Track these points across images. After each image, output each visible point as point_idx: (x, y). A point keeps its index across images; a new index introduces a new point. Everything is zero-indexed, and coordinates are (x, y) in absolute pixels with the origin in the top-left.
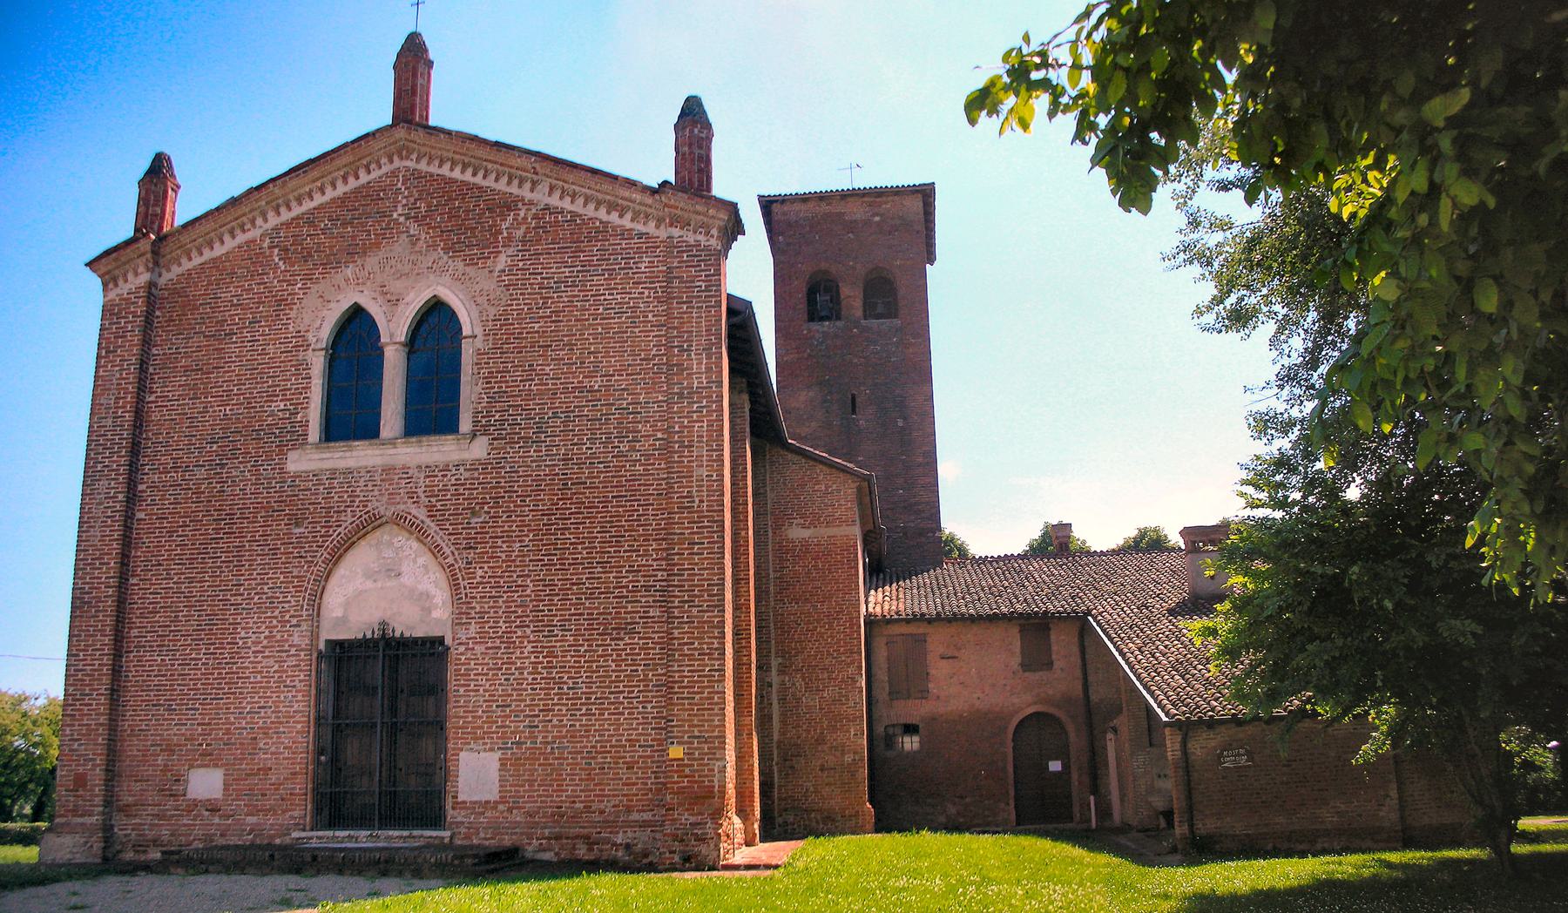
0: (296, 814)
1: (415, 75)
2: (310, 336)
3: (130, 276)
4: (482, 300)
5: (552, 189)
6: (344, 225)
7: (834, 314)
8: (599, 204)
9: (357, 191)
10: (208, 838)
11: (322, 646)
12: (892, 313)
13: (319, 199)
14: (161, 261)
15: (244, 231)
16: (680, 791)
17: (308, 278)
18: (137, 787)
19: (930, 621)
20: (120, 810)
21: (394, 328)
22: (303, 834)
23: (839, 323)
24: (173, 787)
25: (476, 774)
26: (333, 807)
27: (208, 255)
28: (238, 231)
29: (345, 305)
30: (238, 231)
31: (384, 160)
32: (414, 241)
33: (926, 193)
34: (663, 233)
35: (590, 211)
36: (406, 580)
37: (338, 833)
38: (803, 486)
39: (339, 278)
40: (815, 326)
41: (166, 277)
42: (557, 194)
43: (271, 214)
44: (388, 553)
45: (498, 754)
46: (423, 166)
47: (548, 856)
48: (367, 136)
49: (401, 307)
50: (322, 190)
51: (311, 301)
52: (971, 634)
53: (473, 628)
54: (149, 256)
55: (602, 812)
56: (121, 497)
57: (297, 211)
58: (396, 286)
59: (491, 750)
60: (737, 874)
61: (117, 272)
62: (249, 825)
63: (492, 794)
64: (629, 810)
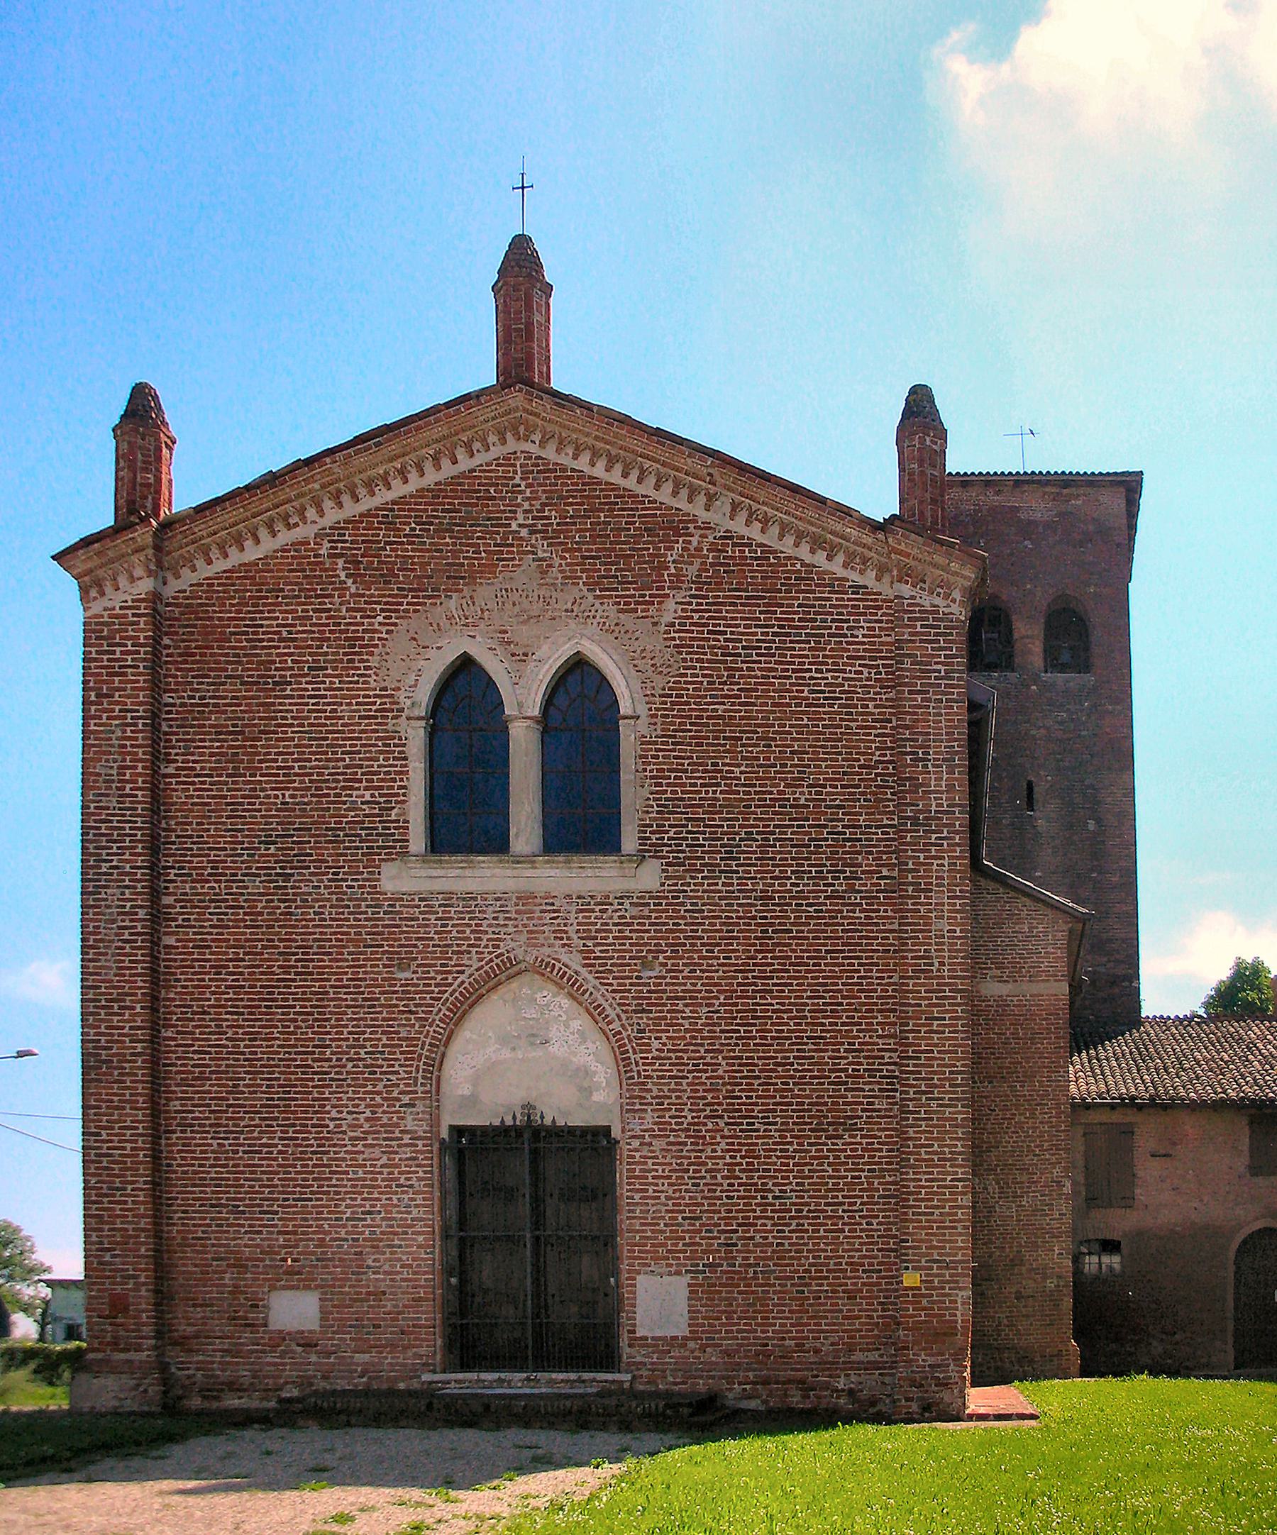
0: (423, 1351)
1: (529, 308)
2: (401, 696)
3: (123, 581)
4: (644, 664)
5: (735, 507)
6: (440, 532)
8: (800, 536)
10: (304, 1382)
11: (445, 1134)
12: (1084, 666)
13: (400, 489)
14: (167, 561)
15: (289, 527)
16: (915, 1328)
17: (392, 608)
18: (199, 1313)
19: (1140, 1107)
20: (175, 1344)
21: (523, 695)
22: (437, 1377)
23: (1013, 676)
24: (249, 1314)
25: (658, 1304)
26: (467, 1345)
27: (235, 558)
28: (279, 526)
29: (450, 655)
30: (279, 526)
31: (492, 438)
33: (1128, 486)
34: (886, 589)
35: (787, 546)
36: (554, 1049)
37: (484, 1376)
38: (1000, 924)
41: (173, 587)
42: (742, 516)
43: (328, 504)
44: (531, 1013)
45: (687, 1279)
46: (550, 453)
47: (753, 1404)
48: (466, 398)
50: (403, 474)
51: (399, 644)
52: (1190, 1125)
53: (650, 1117)
54: (150, 552)
55: (817, 1351)
56: (142, 913)
57: (367, 504)
58: (523, 634)
59: (678, 1273)
60: (983, 1424)
61: (100, 573)
62: (360, 1364)
63: (680, 1327)
64: (851, 1349)
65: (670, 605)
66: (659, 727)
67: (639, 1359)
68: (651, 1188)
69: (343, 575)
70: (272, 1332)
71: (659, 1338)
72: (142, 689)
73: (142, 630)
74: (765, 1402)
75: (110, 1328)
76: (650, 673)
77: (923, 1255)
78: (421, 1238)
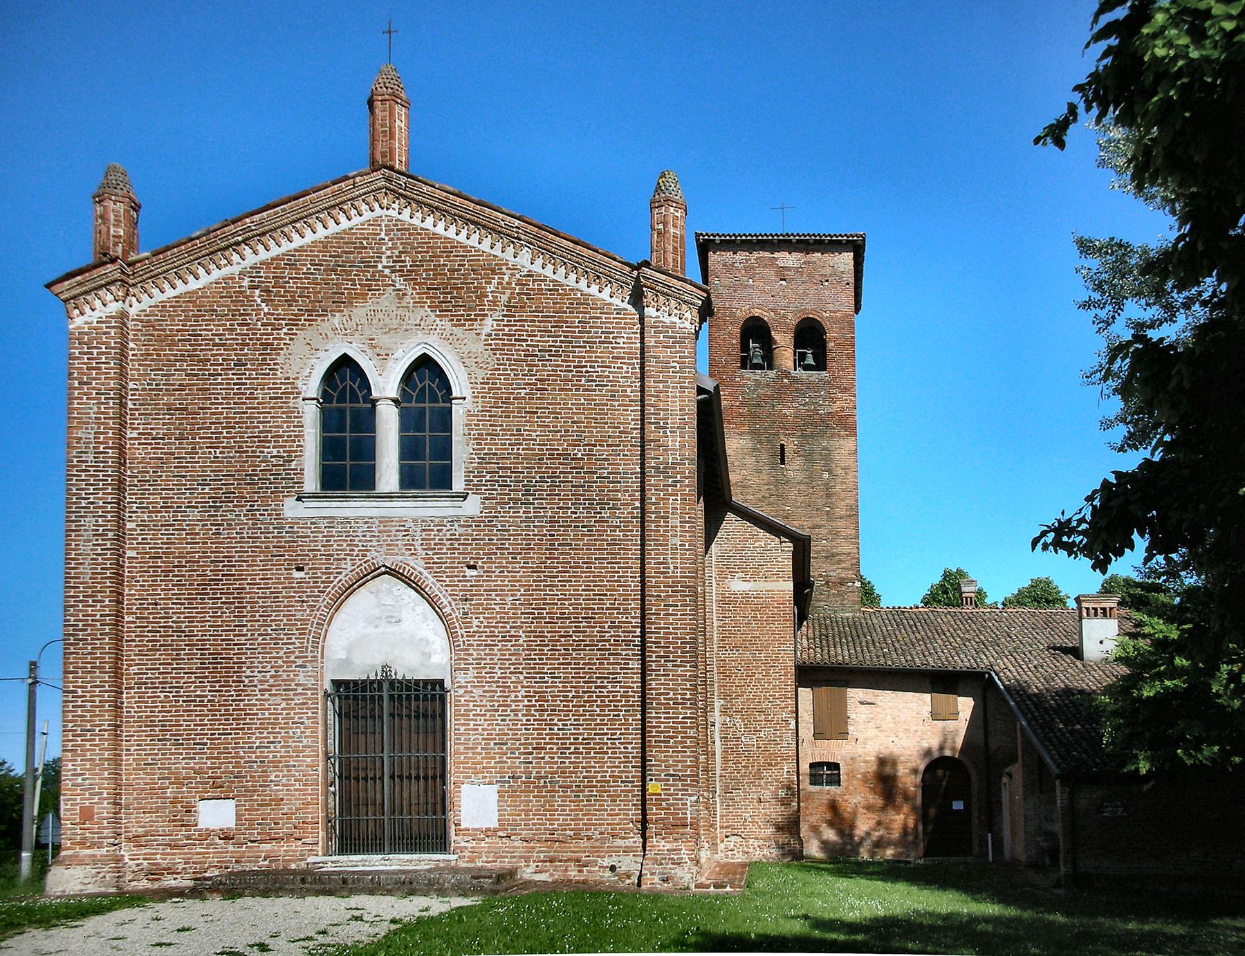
2: (299, 383)
7: (769, 360)
9: (338, 237)
11: (327, 686)
17: (293, 323)
21: (386, 383)
22: (318, 859)
32: (401, 295)
36: (406, 626)
39: (324, 326)
40: (748, 373)
44: (388, 601)
45: (496, 788)
49: (390, 364)
51: (298, 347)
53: (472, 673)
55: (589, 838)
58: (385, 340)
65: (489, 321)
66: (480, 405)
67: (463, 844)
68: (472, 723)
69: (259, 300)
70: (200, 830)
71: (477, 830)
72: (112, 379)
73: (112, 338)
74: (551, 875)
75: (79, 832)
76: (473, 368)
77: (663, 771)
78: (309, 760)
